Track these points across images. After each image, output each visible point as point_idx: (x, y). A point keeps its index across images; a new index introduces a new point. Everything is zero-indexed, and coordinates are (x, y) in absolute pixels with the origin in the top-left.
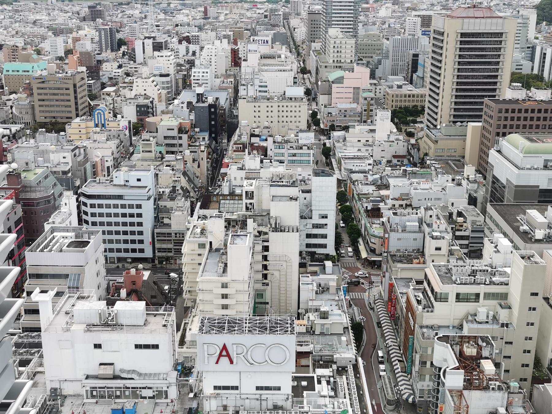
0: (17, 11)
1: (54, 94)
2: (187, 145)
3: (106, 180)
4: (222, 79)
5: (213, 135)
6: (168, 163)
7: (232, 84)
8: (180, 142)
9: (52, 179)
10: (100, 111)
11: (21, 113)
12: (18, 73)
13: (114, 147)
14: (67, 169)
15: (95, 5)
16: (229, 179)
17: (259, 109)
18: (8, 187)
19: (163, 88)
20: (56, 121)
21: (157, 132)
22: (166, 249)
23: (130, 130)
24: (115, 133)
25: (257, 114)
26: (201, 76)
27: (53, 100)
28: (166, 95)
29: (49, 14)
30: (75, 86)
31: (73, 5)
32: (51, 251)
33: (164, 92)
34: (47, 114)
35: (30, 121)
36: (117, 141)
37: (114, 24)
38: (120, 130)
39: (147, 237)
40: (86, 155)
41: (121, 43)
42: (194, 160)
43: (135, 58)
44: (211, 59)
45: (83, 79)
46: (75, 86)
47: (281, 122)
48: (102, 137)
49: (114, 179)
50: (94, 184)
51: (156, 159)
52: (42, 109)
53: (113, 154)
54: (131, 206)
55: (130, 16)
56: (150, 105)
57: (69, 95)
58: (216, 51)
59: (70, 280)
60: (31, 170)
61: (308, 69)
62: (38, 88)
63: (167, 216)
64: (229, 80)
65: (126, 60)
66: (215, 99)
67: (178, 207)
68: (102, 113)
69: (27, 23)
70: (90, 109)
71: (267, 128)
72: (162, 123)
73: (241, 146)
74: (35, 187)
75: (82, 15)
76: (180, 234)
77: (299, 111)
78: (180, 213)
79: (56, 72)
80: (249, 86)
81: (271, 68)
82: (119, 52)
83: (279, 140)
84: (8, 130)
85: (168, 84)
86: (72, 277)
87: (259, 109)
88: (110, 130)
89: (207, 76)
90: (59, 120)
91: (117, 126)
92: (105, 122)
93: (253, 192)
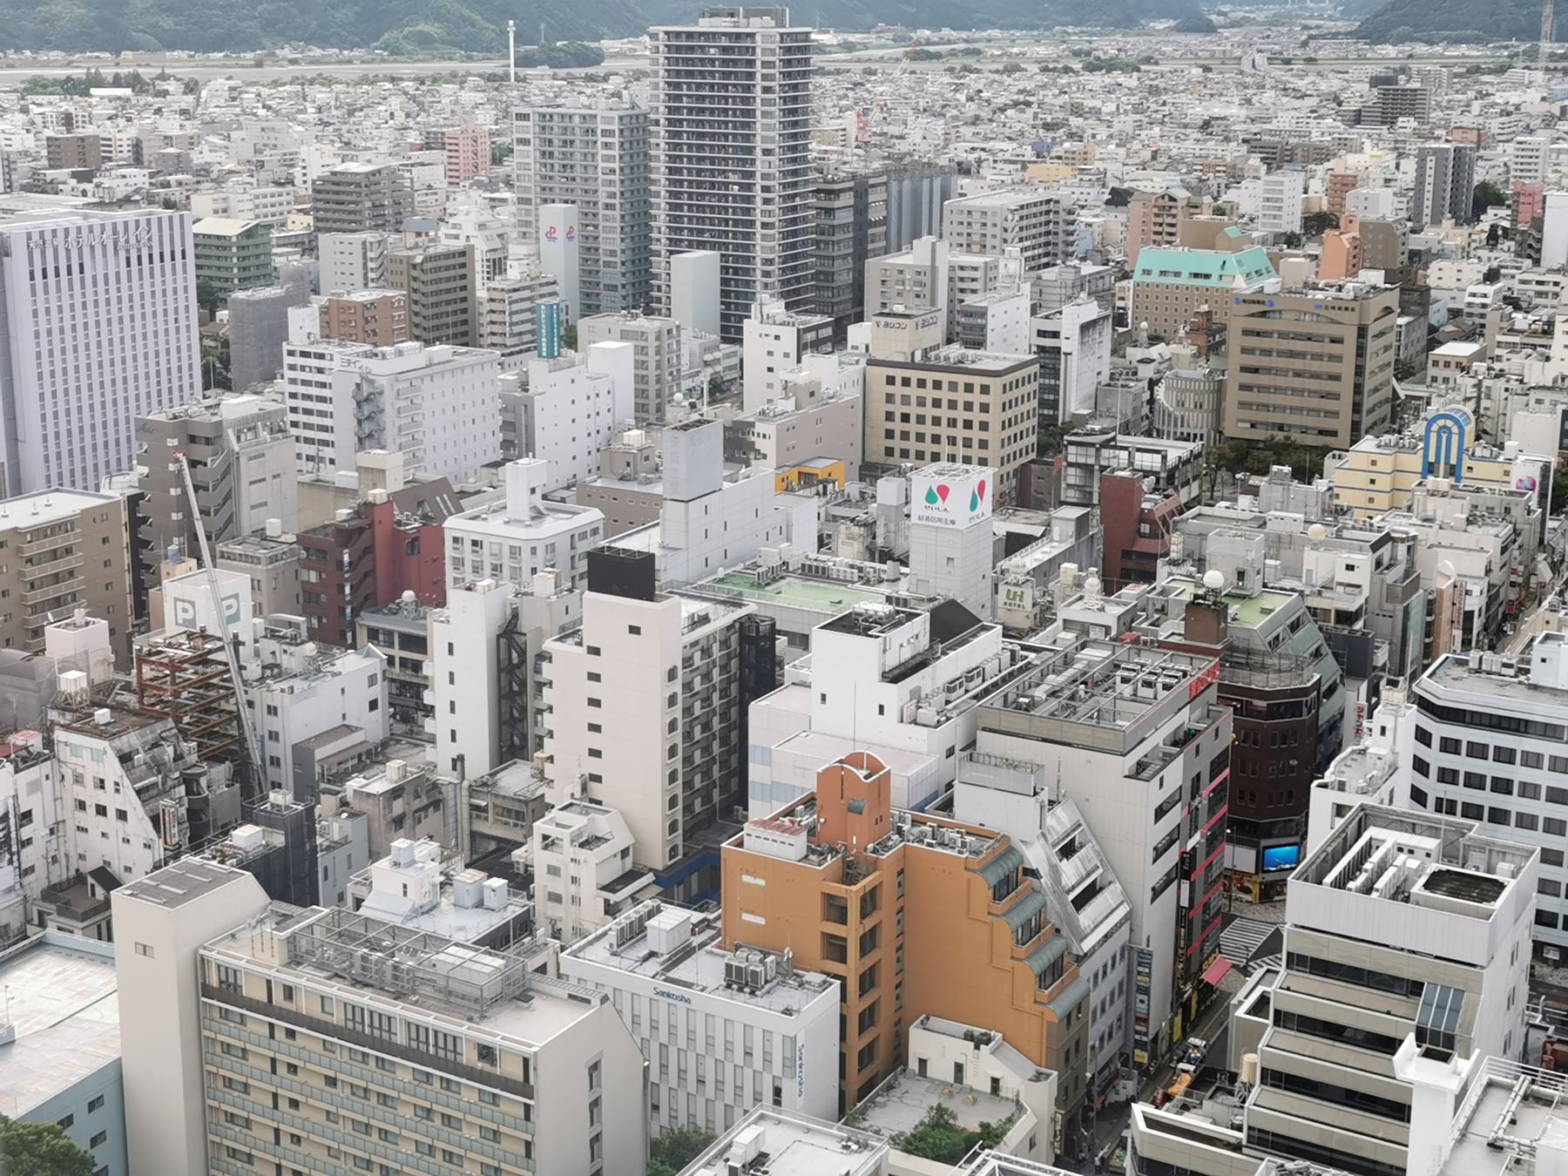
0: (1154, 91)
1: (1292, 354)
3: (1505, 665)
9: (1310, 637)
10: (1449, 423)
12: (1177, 281)
13: (1493, 547)
14: (1353, 608)
15: (1391, 74)
20: (1287, 438)
23: (1543, 496)
24: (1495, 501)
29: (1249, 101)
30: (1362, 331)
31: (1319, 74)
32: (1368, 889)
34: (1261, 416)
35: (1204, 431)
37: (1458, 135)
38: (1511, 493)
41: (1487, 197)
43: (1539, 251)
45: (1388, 311)
46: (1362, 331)
48: (1455, 511)
49: (1535, 666)
50: (1458, 671)
52: (1247, 396)
53: (1488, 571)
55: (1512, 109)
57: (1338, 359)
59: (1427, 1004)
60: (1250, 597)
62: (1246, 332)
65: (1504, 254)
68: (1455, 429)
69: (1186, 126)
70: (1393, 408)
74: (1263, 654)
75: (1352, 106)
79: (1306, 285)
82: (1478, 228)
86: (1431, 994)
88: (1478, 490)
90: (1296, 436)
91: (1499, 476)
92: (1460, 459)
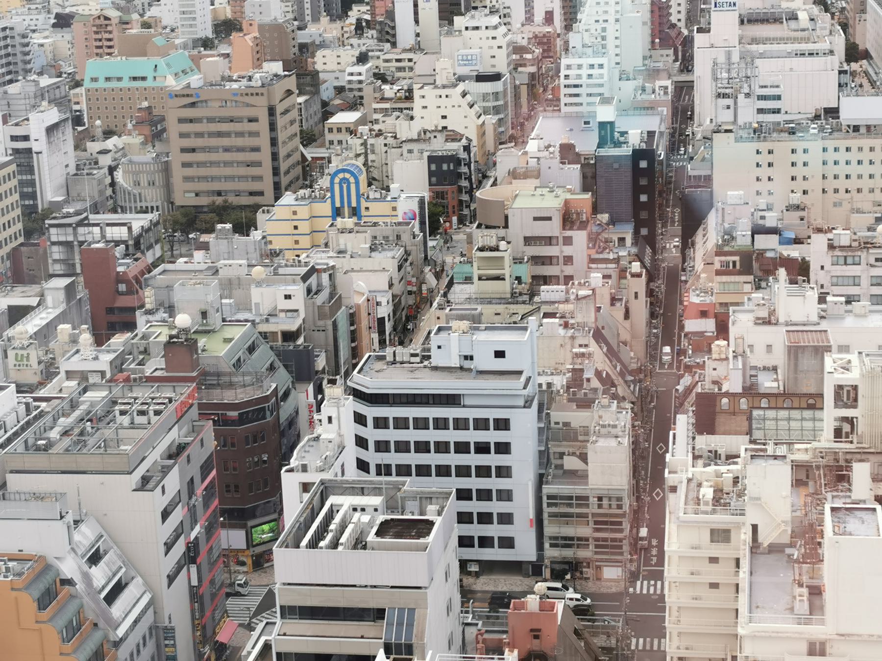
1: (220, 134)
2: (586, 260)
3: (413, 355)
4: (639, 82)
5: (644, 232)
6: (545, 309)
7: (666, 93)
8: (568, 251)
9: (264, 355)
11: (137, 184)
14: (294, 328)
16: (740, 350)
17: (770, 159)
18: (166, 374)
19: (486, 111)
21: (506, 226)
22: (572, 539)
23: (422, 223)
24: (388, 231)
25: (764, 172)
26: (585, 77)
27: (218, 148)
28: (495, 130)
30: (272, 111)
33: (491, 120)
35: (159, 203)
36: (399, 252)
38: (400, 224)
39: (523, 506)
40: (333, 287)
42: (614, 300)
43: (394, 36)
44: (604, 30)
45: (289, 93)
47: (830, 191)
48: (360, 242)
49: (434, 352)
50: (379, 365)
51: (514, 298)
52: (189, 172)
53: (391, 285)
54: (481, 424)
56: (463, 155)
58: (618, 8)
61: (861, 47)
62: (181, 121)
63: (571, 450)
64: (658, 83)
66: (645, 135)
67: (604, 426)
68: (352, 180)
70: (304, 168)
71: (797, 208)
72: (519, 203)
73: (737, 258)
74: (230, 374)
76: (610, 499)
77: (805, 164)
78: (613, 442)
79: (223, 78)
80: (741, 97)
81: (775, 47)
82: (347, 22)
83: (845, 241)
84: (124, 229)
85: (497, 100)
87: (770, 159)
88: (375, 224)
89: (601, 76)
91: (389, 212)
92: (358, 202)
93: (855, 388)
